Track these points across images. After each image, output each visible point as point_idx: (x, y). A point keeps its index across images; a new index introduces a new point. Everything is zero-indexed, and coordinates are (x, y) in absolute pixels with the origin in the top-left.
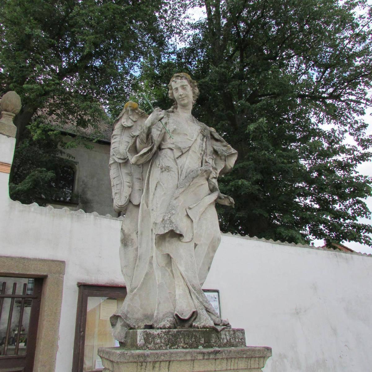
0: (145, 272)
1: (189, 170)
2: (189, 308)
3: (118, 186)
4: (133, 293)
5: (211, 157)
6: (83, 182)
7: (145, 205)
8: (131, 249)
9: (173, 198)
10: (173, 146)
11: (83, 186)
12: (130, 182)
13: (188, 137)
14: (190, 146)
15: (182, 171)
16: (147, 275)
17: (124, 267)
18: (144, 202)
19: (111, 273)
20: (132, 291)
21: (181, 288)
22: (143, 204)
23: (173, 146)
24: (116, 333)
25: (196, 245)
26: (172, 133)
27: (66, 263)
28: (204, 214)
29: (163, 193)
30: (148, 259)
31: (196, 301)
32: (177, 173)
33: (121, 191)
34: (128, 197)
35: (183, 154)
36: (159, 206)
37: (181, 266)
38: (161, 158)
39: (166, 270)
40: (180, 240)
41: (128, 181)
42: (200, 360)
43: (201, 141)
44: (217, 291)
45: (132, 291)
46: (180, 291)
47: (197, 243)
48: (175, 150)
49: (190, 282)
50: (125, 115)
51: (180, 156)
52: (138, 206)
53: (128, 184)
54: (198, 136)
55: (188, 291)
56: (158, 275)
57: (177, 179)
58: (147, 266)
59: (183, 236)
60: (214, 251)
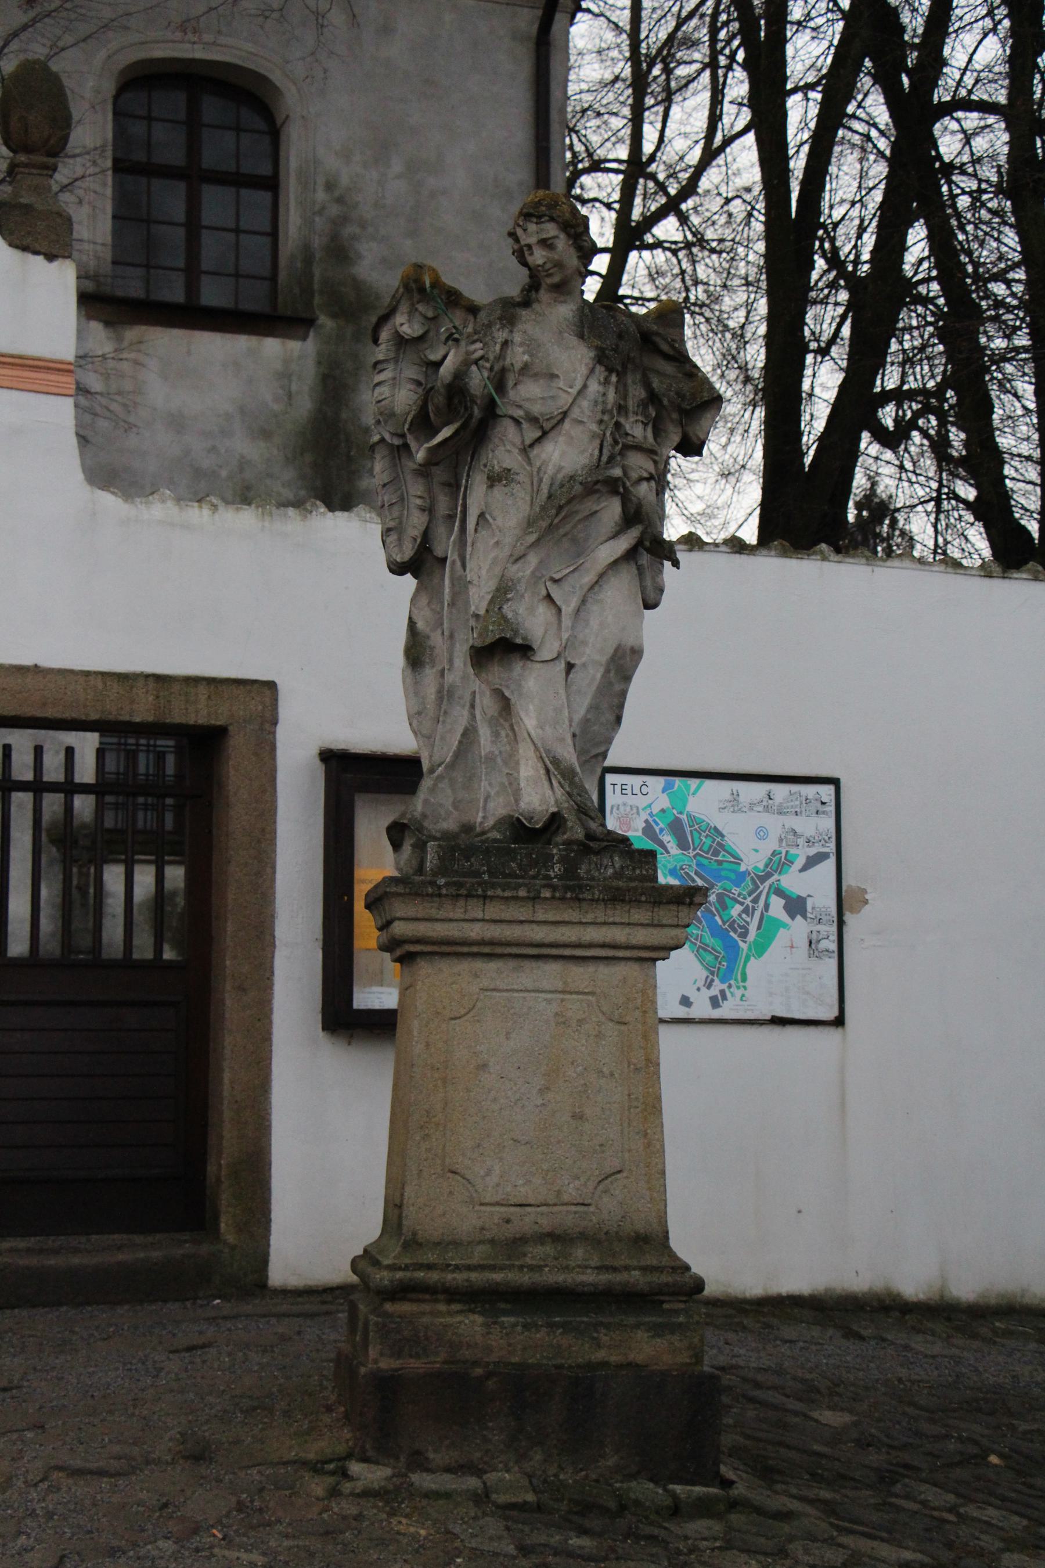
0: (460, 730)
1: (560, 476)
2: (544, 807)
3: (396, 508)
4: (436, 774)
5: (640, 418)
6: (330, 186)
7: (458, 564)
8: (429, 674)
9: (511, 560)
10: (521, 413)
11: (334, 210)
12: (426, 495)
13: (561, 384)
14: (565, 409)
15: (541, 480)
16: (465, 733)
17: (415, 717)
18: (456, 557)
19: (388, 731)
20: (432, 771)
21: (530, 762)
22: (454, 562)
23: (521, 413)
24: (402, 863)
25: (570, 667)
26: (519, 375)
27: (279, 687)
28: (596, 588)
29: (492, 542)
30: (468, 698)
31: (559, 792)
32: (529, 487)
33: (401, 523)
34: (419, 540)
35: (545, 434)
36: (484, 572)
37: (529, 720)
38: (491, 446)
39: (502, 725)
40: (528, 659)
41: (419, 493)
42: (546, 899)
43: (601, 389)
44: (835, 782)
45: (432, 771)
46: (529, 769)
47: (572, 662)
48: (525, 425)
49: (548, 751)
50: (403, 302)
51: (539, 440)
52: (445, 559)
53: (419, 502)
54: (592, 371)
55: (542, 771)
56: (484, 733)
57: (529, 502)
58: (466, 713)
59: (533, 650)
60: (627, 679)
